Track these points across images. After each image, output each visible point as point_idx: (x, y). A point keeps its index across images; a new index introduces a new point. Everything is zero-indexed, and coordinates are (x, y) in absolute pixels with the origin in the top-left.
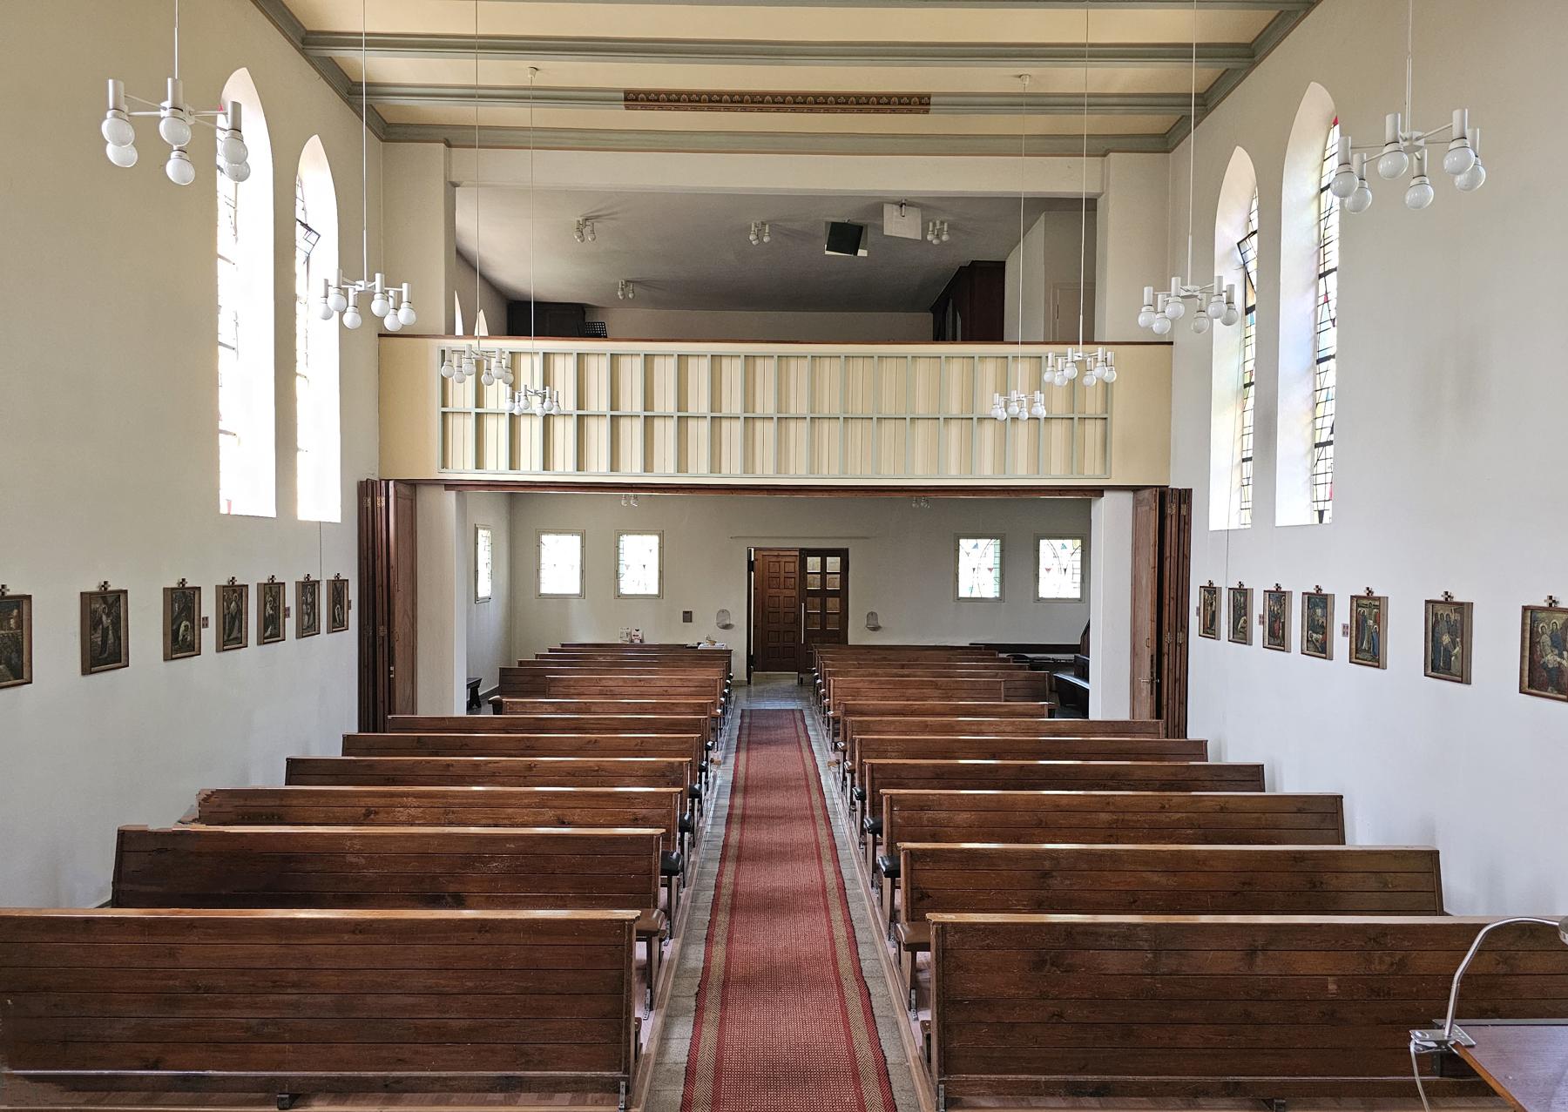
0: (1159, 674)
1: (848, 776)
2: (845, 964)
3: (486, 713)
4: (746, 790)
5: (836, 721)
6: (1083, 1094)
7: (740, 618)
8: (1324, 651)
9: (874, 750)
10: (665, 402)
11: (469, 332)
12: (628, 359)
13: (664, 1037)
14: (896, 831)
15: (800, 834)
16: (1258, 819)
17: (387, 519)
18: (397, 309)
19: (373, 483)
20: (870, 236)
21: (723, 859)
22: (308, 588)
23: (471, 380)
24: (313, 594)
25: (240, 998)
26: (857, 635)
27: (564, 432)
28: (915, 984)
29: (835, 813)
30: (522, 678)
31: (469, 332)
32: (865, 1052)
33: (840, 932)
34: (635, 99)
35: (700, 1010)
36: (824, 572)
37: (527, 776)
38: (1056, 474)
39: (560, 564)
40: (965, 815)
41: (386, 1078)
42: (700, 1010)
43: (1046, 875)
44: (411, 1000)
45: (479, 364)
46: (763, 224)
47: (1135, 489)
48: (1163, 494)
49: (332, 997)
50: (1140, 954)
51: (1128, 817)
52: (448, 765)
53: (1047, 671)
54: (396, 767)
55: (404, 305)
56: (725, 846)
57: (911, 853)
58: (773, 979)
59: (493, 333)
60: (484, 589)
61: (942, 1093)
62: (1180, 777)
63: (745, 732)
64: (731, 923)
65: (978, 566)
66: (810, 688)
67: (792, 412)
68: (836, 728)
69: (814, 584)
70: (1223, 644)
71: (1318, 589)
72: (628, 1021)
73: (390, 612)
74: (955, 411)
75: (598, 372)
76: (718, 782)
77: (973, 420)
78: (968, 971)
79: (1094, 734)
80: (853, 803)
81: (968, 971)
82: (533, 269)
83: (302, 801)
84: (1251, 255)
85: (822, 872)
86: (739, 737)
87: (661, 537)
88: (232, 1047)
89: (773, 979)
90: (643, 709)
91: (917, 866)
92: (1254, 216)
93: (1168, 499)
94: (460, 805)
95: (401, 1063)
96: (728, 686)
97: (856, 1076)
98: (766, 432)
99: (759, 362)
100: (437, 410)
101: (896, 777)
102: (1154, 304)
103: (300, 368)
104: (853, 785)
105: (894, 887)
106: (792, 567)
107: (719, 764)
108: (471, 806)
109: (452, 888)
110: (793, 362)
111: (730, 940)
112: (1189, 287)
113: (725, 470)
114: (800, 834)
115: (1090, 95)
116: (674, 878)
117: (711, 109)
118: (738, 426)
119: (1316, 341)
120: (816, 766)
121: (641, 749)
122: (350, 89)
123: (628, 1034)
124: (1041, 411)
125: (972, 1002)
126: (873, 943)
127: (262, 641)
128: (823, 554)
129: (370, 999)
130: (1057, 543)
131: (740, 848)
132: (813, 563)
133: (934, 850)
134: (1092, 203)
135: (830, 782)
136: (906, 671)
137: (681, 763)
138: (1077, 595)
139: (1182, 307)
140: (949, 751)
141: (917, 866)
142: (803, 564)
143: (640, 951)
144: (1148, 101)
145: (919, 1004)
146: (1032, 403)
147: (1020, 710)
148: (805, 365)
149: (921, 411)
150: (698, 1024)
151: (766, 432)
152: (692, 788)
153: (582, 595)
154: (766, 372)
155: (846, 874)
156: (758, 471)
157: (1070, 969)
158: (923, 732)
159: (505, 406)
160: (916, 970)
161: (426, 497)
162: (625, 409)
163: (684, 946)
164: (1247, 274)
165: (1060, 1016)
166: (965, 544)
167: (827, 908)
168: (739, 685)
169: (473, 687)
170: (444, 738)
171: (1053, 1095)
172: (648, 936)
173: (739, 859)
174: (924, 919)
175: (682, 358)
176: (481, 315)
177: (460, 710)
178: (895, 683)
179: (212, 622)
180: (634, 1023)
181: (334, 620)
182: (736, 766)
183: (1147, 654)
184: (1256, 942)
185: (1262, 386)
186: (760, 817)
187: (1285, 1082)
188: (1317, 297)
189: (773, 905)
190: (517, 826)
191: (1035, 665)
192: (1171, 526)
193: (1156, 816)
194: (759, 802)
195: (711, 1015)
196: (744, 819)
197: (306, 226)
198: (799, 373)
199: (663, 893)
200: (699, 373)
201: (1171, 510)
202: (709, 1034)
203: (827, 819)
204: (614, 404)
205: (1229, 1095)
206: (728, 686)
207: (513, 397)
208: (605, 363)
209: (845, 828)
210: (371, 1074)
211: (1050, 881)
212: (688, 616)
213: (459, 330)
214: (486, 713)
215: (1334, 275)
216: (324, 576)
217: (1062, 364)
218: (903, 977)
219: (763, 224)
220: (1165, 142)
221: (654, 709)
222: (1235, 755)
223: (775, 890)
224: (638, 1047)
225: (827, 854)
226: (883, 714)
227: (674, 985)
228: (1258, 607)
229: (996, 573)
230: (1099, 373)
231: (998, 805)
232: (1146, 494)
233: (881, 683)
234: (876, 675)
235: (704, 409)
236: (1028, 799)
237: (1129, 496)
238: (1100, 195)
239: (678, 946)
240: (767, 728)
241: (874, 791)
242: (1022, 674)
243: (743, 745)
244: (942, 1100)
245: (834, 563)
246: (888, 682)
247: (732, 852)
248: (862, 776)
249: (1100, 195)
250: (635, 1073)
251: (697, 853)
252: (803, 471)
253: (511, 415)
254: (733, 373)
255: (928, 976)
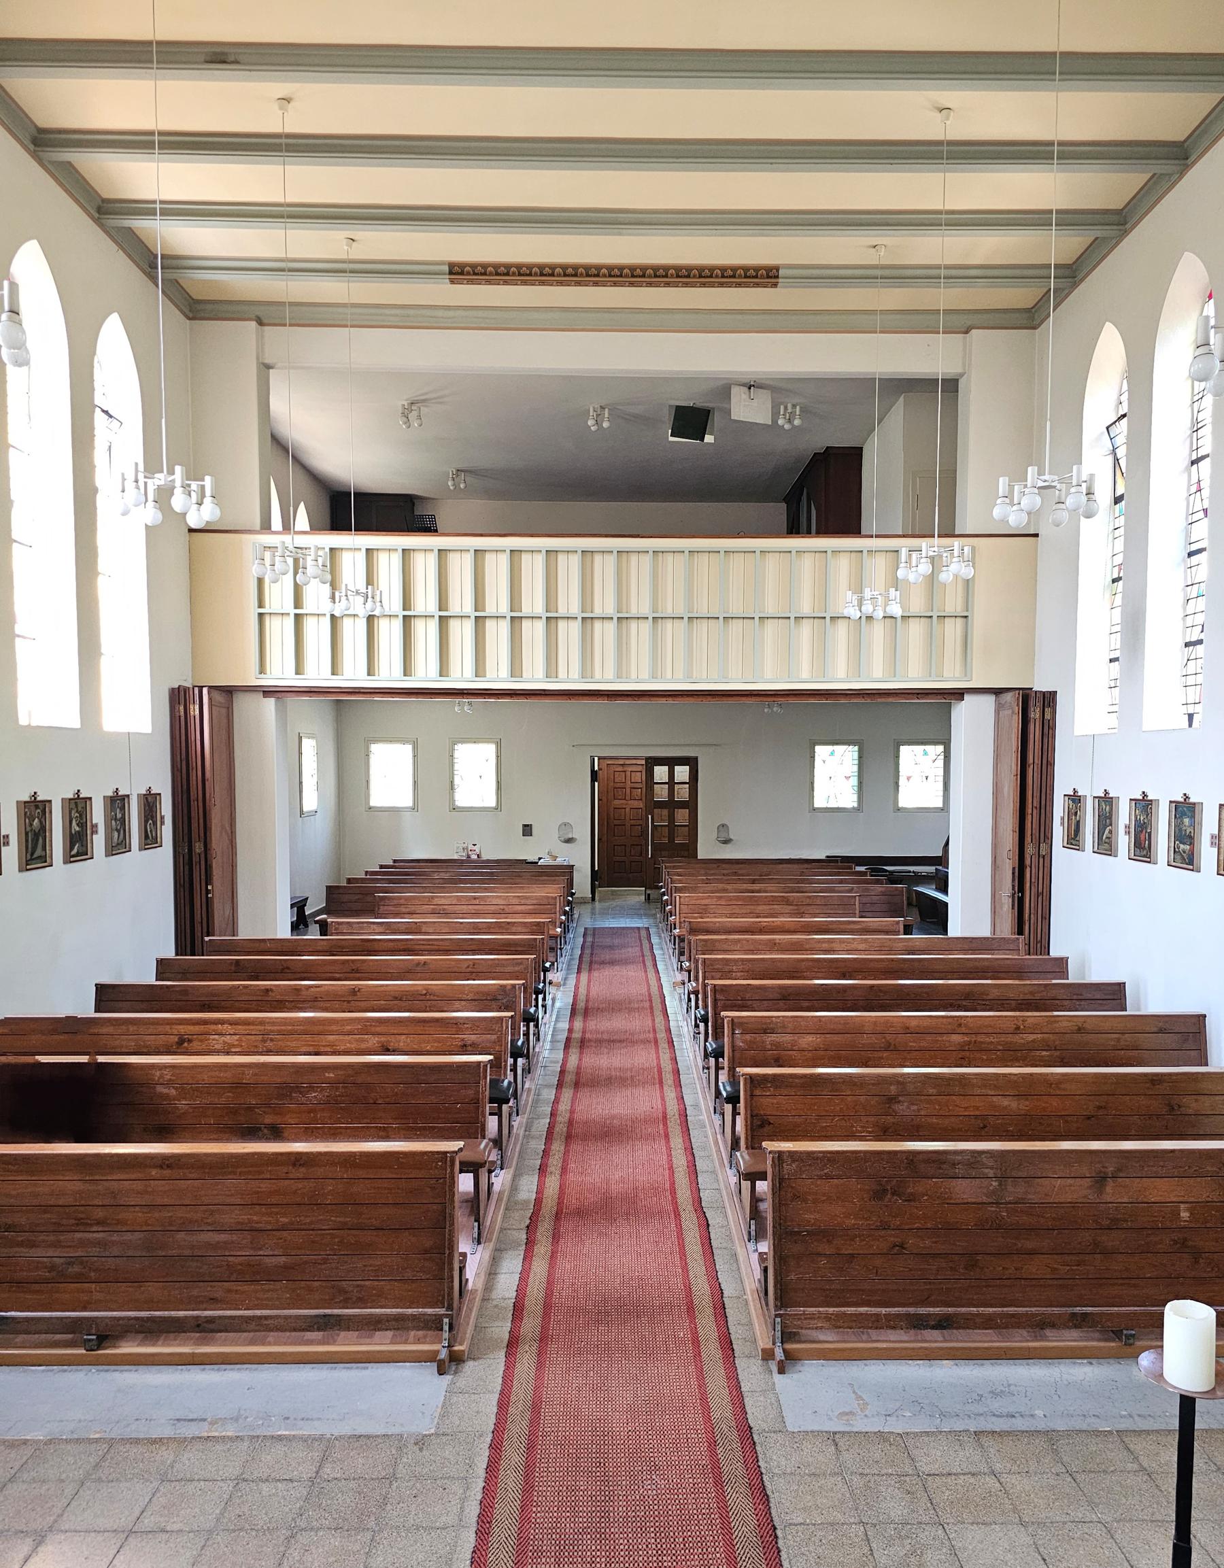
0: (1021, 889)
1: (693, 997)
2: (684, 1194)
3: (313, 934)
4: (586, 1012)
5: (682, 940)
6: (926, 1327)
7: (583, 832)
8: (1191, 862)
9: (718, 970)
10: (497, 601)
11: (287, 527)
12: (493, 555)
13: (492, 1273)
14: (737, 1055)
15: (642, 1058)
16: (1118, 1040)
17: (201, 727)
18: (200, 504)
19: (186, 690)
20: (717, 420)
21: (560, 1085)
22: (117, 802)
23: (288, 580)
24: (123, 808)
25: (42, 1237)
26: (706, 850)
27: (390, 633)
28: (755, 1214)
29: (680, 1035)
30: (349, 897)
31: (287, 527)
32: (701, 1287)
33: (680, 1161)
34: (460, 272)
35: (530, 1243)
36: (671, 782)
37: (351, 1000)
38: (914, 676)
39: (390, 774)
40: (810, 1038)
41: (197, 1317)
42: (530, 1243)
43: (892, 1100)
44: (223, 1237)
45: (296, 561)
46: (602, 408)
47: (997, 692)
48: (1026, 697)
49: (142, 1235)
50: (985, 1182)
51: (980, 1038)
52: (267, 991)
53: (909, 887)
54: (214, 992)
55: (208, 500)
56: (562, 1072)
57: (752, 1079)
58: (604, 1210)
59: (315, 528)
60: (310, 802)
61: (778, 1327)
62: (1038, 996)
63: (588, 951)
64: (566, 1152)
65: (835, 774)
66: (656, 903)
67: (634, 612)
68: (682, 948)
69: (661, 793)
70: (1088, 857)
71: (1186, 797)
72: (451, 1256)
73: (206, 829)
74: (806, 608)
75: (425, 567)
76: (558, 1004)
77: (827, 619)
78: (805, 1201)
79: (950, 951)
80: (697, 1026)
81: (805, 1201)
82: (359, 456)
83: (110, 1030)
84: (1120, 440)
85: (663, 1099)
86: (581, 957)
87: (499, 746)
88: (36, 1287)
89: (604, 1210)
90: (476, 929)
91: (757, 1092)
92: (1125, 398)
93: (1031, 703)
94: (280, 1033)
95: (214, 1302)
96: (569, 903)
97: (691, 1309)
98: (605, 633)
99: (598, 558)
100: (254, 611)
101: (739, 999)
102: (1009, 496)
103: (101, 566)
104: (697, 1007)
105: (735, 1113)
106: (639, 777)
107: (558, 985)
108: (291, 1033)
109: (268, 1119)
110: (634, 558)
111: (564, 1170)
112: (1046, 477)
113: (562, 674)
114: (642, 1058)
115: (947, 267)
116: (505, 1107)
117: (543, 283)
118: (575, 626)
119: (1188, 534)
120: (661, 987)
121: (474, 971)
122: (148, 260)
123: (451, 1270)
124: (896, 610)
125: (810, 1233)
126: (714, 1172)
127: (69, 859)
128: (671, 762)
129: (181, 1235)
130: (919, 749)
131: (578, 1074)
132: (661, 772)
133: (775, 1075)
134: (951, 385)
135: (675, 1004)
136: (756, 886)
137: (514, 986)
138: (941, 805)
139: (1038, 499)
140: (794, 971)
141: (757, 1092)
142: (650, 774)
143: (465, 1183)
144: (1018, 272)
145: (759, 1236)
146: (887, 600)
147: (875, 926)
148: (647, 560)
149: (770, 610)
150: (528, 1257)
151: (605, 633)
152: (526, 1012)
153: (414, 808)
154: (605, 568)
155: (688, 1100)
156: (598, 675)
157: (911, 1198)
158: (771, 951)
159: (326, 607)
160: (755, 1200)
161: (243, 704)
162: (454, 608)
163: (516, 1177)
164: (1116, 460)
165: (902, 1246)
166: (821, 751)
167: (667, 1136)
168: (583, 902)
169: (299, 906)
170: (267, 960)
171: (894, 1328)
172: (472, 1167)
173: (577, 1085)
174: (761, 1146)
175: (479, 553)
176: (302, 509)
177: (283, 930)
178: (744, 898)
179: (14, 840)
180: (456, 1256)
181: (147, 837)
182: (577, 987)
183: (1008, 867)
184: (1104, 1170)
185: (1129, 579)
186: (600, 1042)
187: (1135, 1313)
188: (1190, 485)
189: (610, 1134)
190: (326, 1054)
191: (893, 879)
192: (1035, 731)
193: (1010, 1038)
194: (602, 1025)
195: (542, 1248)
196: (583, 1043)
197: (106, 412)
198: (640, 568)
199: (492, 1123)
200: (533, 568)
201: (1035, 714)
202: (539, 1268)
203: (671, 1043)
204: (443, 603)
205: (1076, 1327)
206: (569, 903)
207: (333, 598)
208: (432, 559)
209: (689, 1051)
210: (181, 1313)
211: (896, 1107)
212: (527, 830)
213: (277, 523)
214: (313, 934)
215: (1207, 461)
216: (134, 790)
217: (917, 560)
218: (743, 1208)
219: (602, 408)
220: (1030, 318)
221: (489, 928)
222: (1099, 974)
223: (613, 1117)
224: (463, 1283)
225: (668, 1078)
226: (729, 932)
227: (504, 1217)
228: (1124, 816)
229: (854, 781)
230: (955, 570)
231: (845, 1028)
232: (1008, 697)
233: (730, 899)
234: (725, 891)
235: (539, 608)
236: (875, 1022)
237: (990, 700)
238: (962, 375)
239: (509, 1177)
240: (611, 947)
241: (716, 1014)
242: (879, 888)
243: (585, 966)
244: (779, 1334)
245: (682, 773)
246: (738, 898)
247: (569, 1078)
248: (705, 997)
249: (962, 375)
250: (460, 1309)
251: (532, 1080)
252: (645, 675)
253: (332, 616)
254: (569, 568)
255: (766, 1207)
